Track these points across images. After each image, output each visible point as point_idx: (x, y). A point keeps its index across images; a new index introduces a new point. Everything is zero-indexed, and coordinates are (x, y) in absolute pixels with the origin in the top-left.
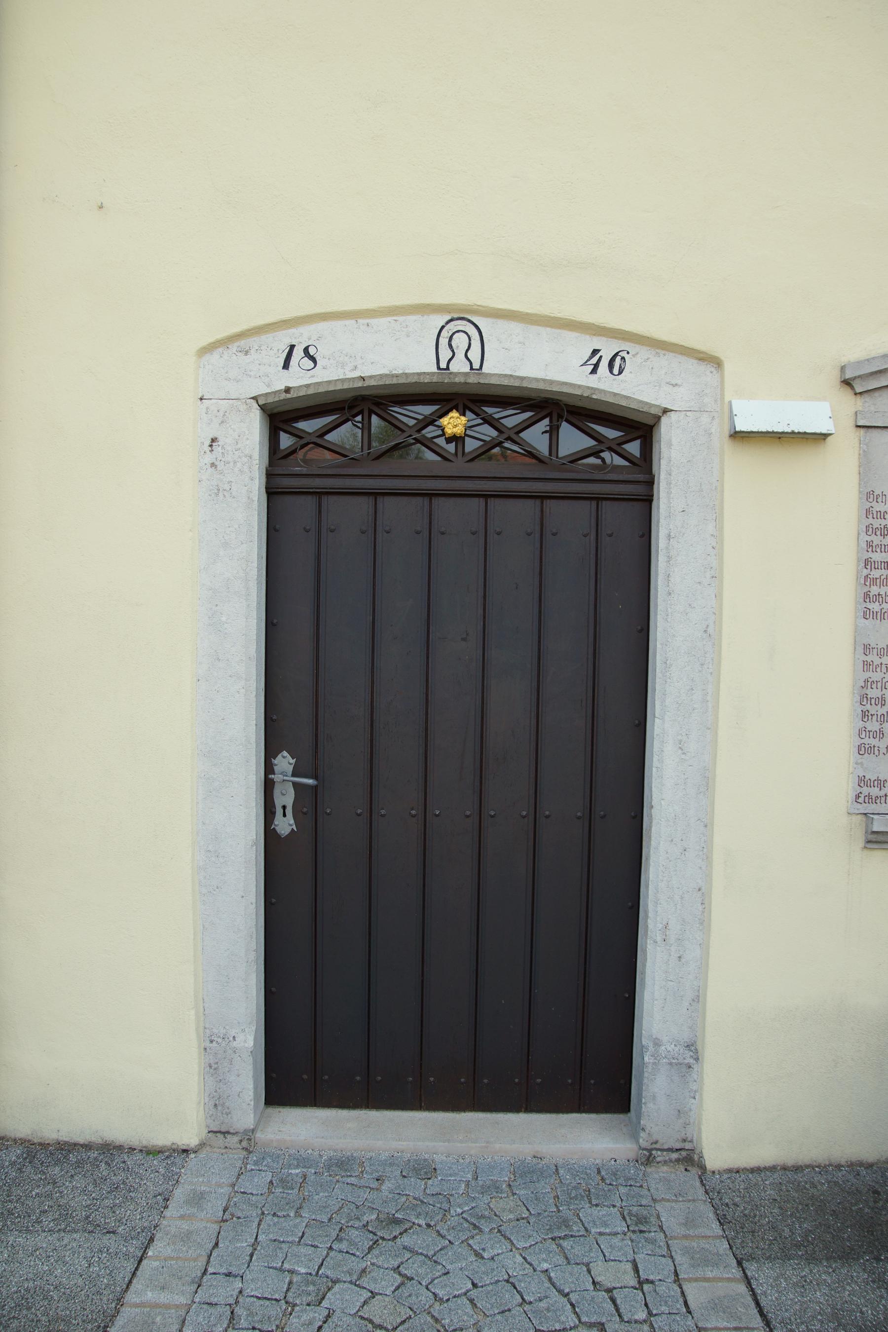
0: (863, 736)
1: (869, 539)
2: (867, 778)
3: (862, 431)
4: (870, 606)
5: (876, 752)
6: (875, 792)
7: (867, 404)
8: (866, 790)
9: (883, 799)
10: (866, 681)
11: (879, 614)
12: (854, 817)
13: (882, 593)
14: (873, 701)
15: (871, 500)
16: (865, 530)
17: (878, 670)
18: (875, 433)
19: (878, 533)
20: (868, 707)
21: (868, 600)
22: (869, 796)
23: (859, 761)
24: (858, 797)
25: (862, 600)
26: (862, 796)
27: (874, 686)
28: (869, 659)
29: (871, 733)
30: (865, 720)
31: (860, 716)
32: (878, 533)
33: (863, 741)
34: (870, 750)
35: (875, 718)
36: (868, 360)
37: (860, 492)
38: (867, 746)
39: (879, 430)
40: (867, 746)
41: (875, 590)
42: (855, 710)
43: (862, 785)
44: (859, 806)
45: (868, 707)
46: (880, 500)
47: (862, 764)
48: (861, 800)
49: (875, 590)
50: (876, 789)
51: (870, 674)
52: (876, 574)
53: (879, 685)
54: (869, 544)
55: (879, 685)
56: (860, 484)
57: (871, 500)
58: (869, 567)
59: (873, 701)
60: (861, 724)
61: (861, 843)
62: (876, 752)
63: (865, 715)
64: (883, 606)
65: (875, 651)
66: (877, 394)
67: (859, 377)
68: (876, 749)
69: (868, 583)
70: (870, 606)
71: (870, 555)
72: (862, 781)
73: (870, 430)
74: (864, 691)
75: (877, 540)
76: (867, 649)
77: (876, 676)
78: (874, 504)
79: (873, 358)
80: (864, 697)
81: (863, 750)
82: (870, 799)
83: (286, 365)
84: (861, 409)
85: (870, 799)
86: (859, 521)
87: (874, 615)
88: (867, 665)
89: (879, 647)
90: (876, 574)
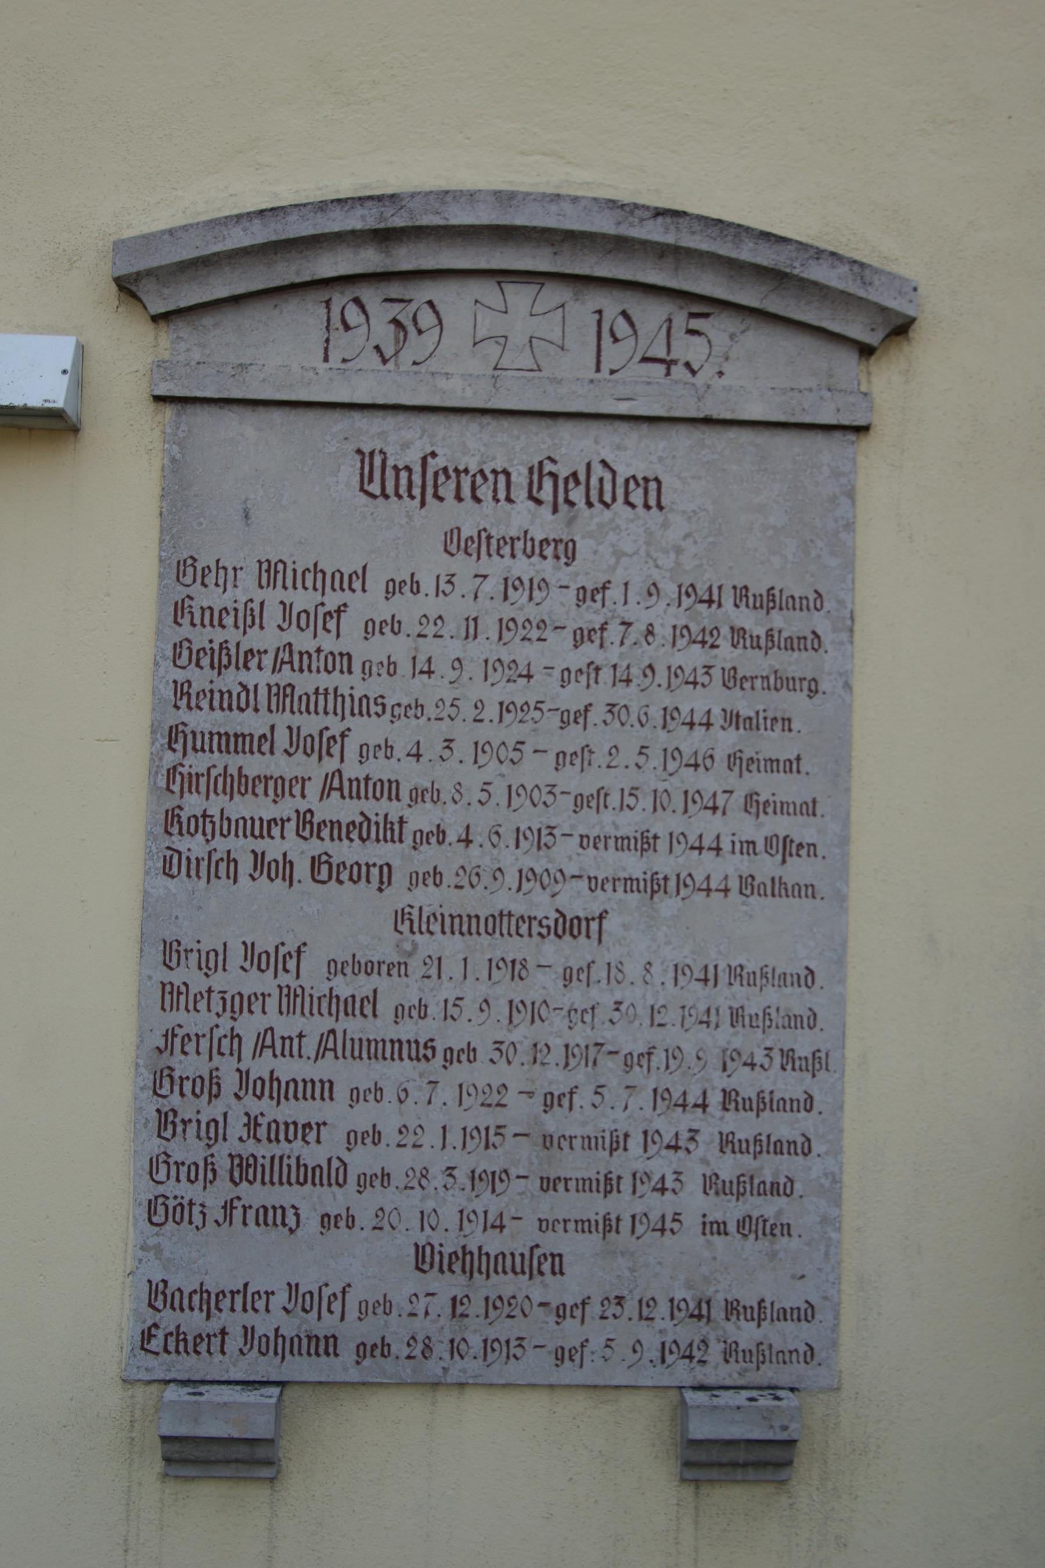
0: (162, 1176)
1: (180, 675)
2: (173, 1285)
3: (169, 412)
4: (182, 844)
5: (197, 1218)
6: (194, 1322)
7: (183, 346)
8: (168, 1319)
9: (216, 1342)
10: (169, 1035)
11: (204, 865)
12: (140, 1391)
13: (214, 811)
14: (188, 1086)
15: (188, 580)
16: (170, 653)
17: (202, 1005)
18: (202, 416)
19: (205, 662)
20: (175, 1100)
21: (175, 830)
22: (178, 1333)
23: (151, 1242)
24: (147, 1336)
25: (160, 829)
26: (160, 1334)
27: (190, 1047)
28: (177, 977)
29: (184, 1170)
30: (168, 1134)
31: (154, 1125)
32: (205, 662)
33: (161, 1189)
34: (180, 1212)
35: (192, 1129)
36: (171, 232)
37: (161, 561)
38: (171, 1203)
39: (214, 410)
40: (171, 1203)
41: (193, 804)
42: (140, 1110)
43: (159, 1304)
44: (150, 1361)
45: (175, 1100)
46: (210, 580)
47: (158, 1249)
48: (156, 1344)
49: (193, 804)
50: (198, 1316)
51: (181, 1016)
52: (197, 763)
53: (204, 1044)
54: (182, 690)
55: (204, 1044)
56: (161, 541)
57: (188, 580)
58: (179, 746)
59: (188, 1086)
60: (155, 1145)
61: (159, 1466)
62: (197, 1218)
63: (166, 1122)
64: (213, 844)
65: (193, 957)
66: (208, 321)
67: (149, 273)
68: (196, 1210)
69: (176, 788)
70: (182, 844)
71: (184, 715)
72: (159, 1294)
73: (190, 409)
74: (165, 1060)
75: (200, 679)
76: (172, 952)
77: (197, 1022)
78: (196, 589)
79: (185, 228)
80: (162, 1079)
81: (160, 1212)
82: (181, 1342)
83: (225, 944)
84: (167, 356)
85: (181, 1342)
86: (159, 633)
87: (192, 867)
88: (171, 995)
89: (204, 947)
90: (197, 763)
